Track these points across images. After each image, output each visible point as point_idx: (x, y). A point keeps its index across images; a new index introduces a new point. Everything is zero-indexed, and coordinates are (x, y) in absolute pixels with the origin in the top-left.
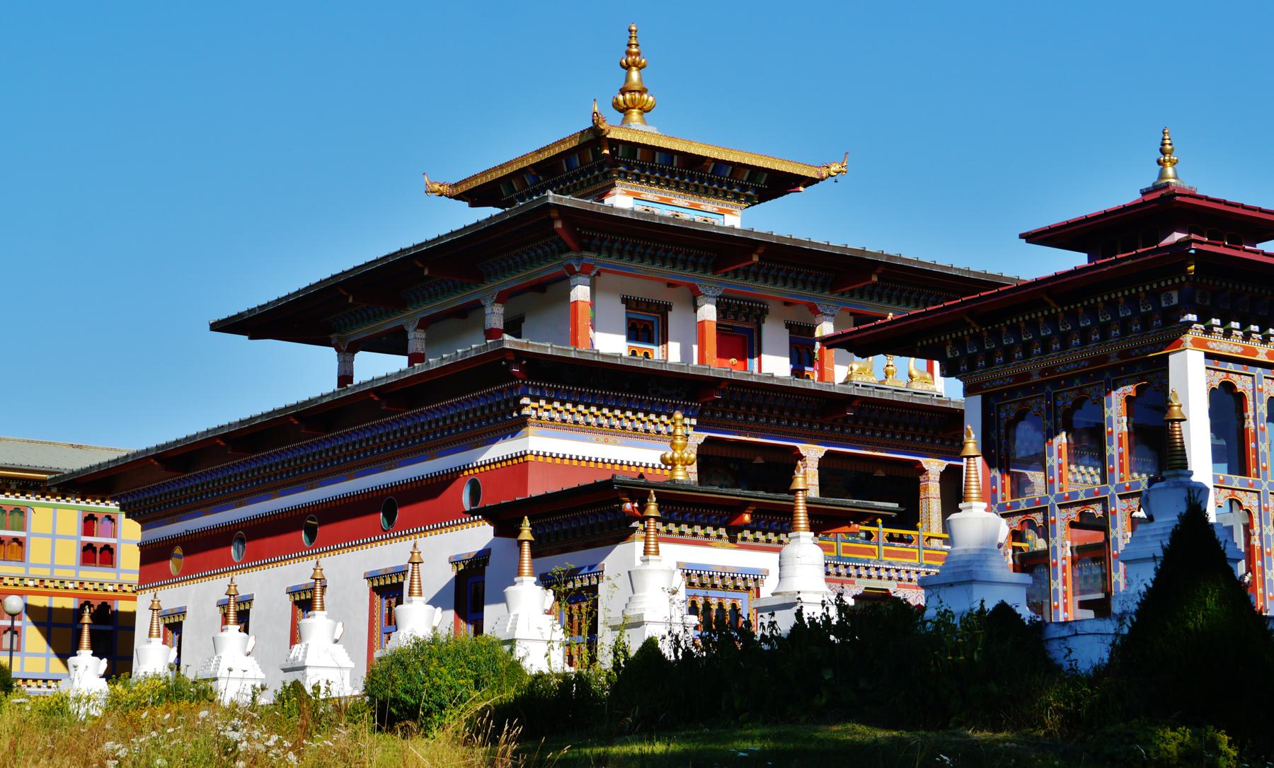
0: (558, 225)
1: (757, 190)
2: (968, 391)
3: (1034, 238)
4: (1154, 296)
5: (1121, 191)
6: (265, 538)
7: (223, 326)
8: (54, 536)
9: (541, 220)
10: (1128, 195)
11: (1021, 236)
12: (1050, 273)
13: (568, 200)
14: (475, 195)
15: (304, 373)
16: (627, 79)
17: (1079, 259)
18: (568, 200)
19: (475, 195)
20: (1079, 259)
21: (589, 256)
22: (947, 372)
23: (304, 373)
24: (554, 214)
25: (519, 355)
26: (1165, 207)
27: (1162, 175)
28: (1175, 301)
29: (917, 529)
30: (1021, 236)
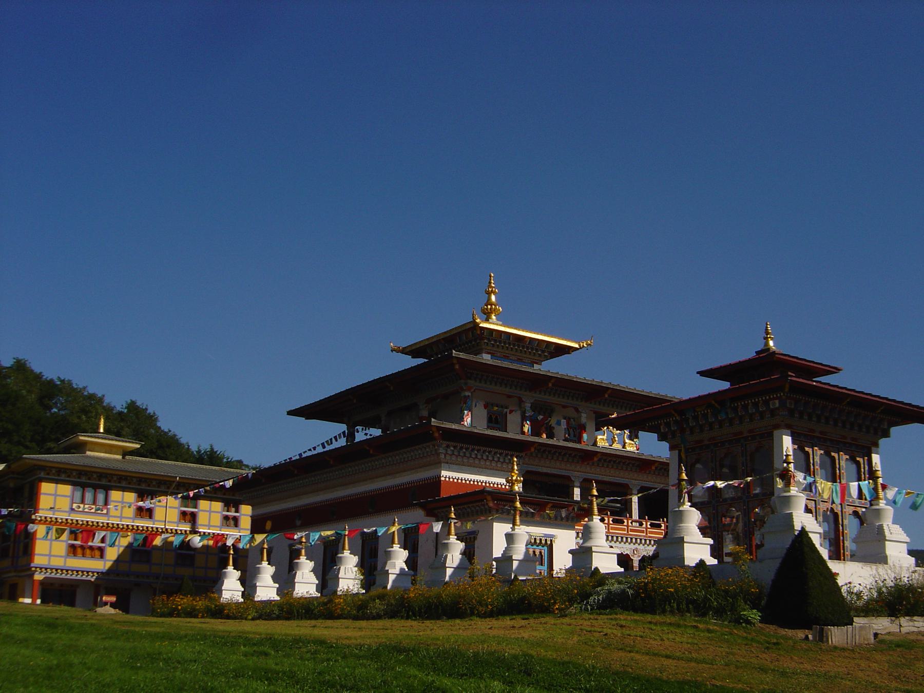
0: (457, 367)
1: (550, 353)
2: (672, 448)
3: (702, 373)
4: (766, 403)
5: (746, 353)
6: (313, 517)
7: (290, 413)
8: (210, 512)
9: (450, 366)
10: (749, 354)
11: (698, 373)
12: (717, 390)
13: (462, 355)
14: (413, 351)
15: (325, 435)
16: (489, 298)
17: (725, 385)
18: (462, 355)
19: (413, 351)
20: (725, 385)
21: (471, 382)
22: (662, 438)
23: (325, 435)
24: (455, 361)
25: (438, 428)
26: (766, 362)
27: (767, 344)
28: (777, 405)
29: (641, 516)
30: (698, 373)
